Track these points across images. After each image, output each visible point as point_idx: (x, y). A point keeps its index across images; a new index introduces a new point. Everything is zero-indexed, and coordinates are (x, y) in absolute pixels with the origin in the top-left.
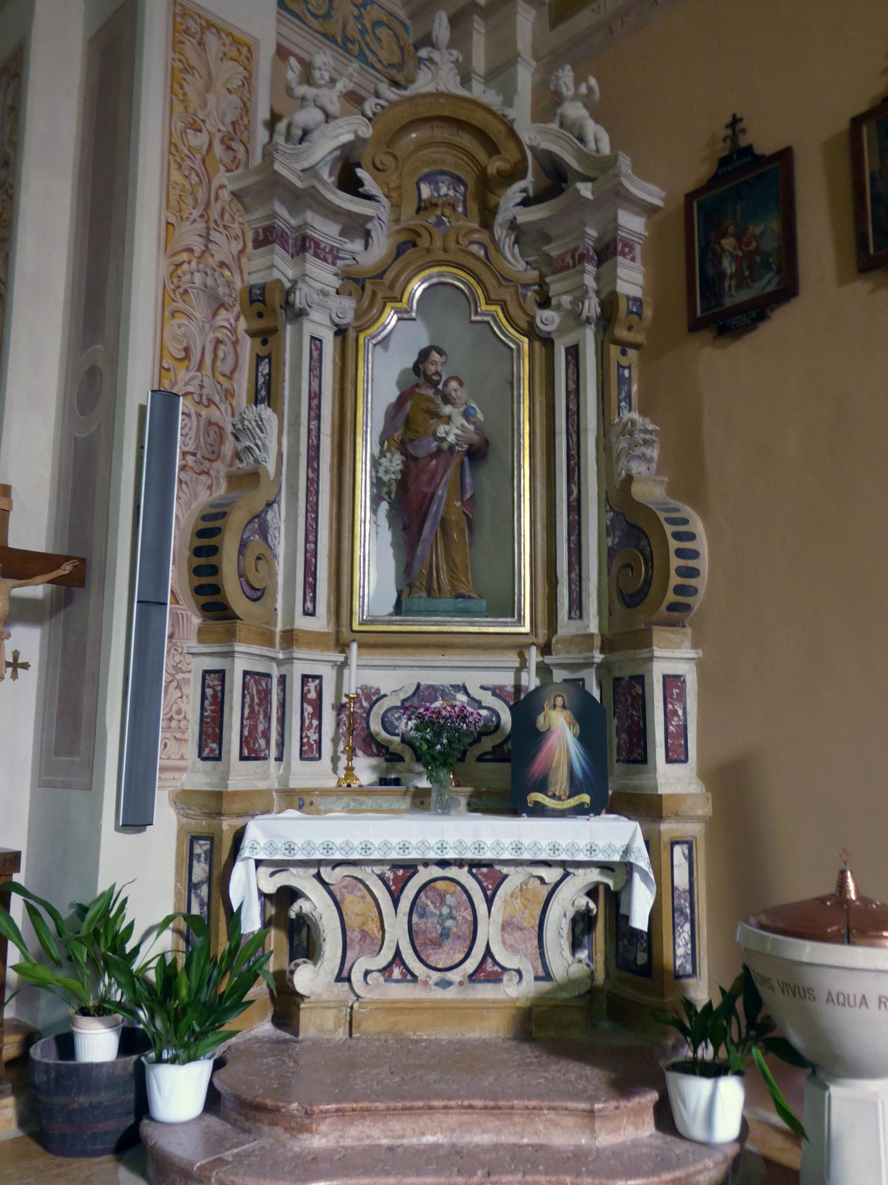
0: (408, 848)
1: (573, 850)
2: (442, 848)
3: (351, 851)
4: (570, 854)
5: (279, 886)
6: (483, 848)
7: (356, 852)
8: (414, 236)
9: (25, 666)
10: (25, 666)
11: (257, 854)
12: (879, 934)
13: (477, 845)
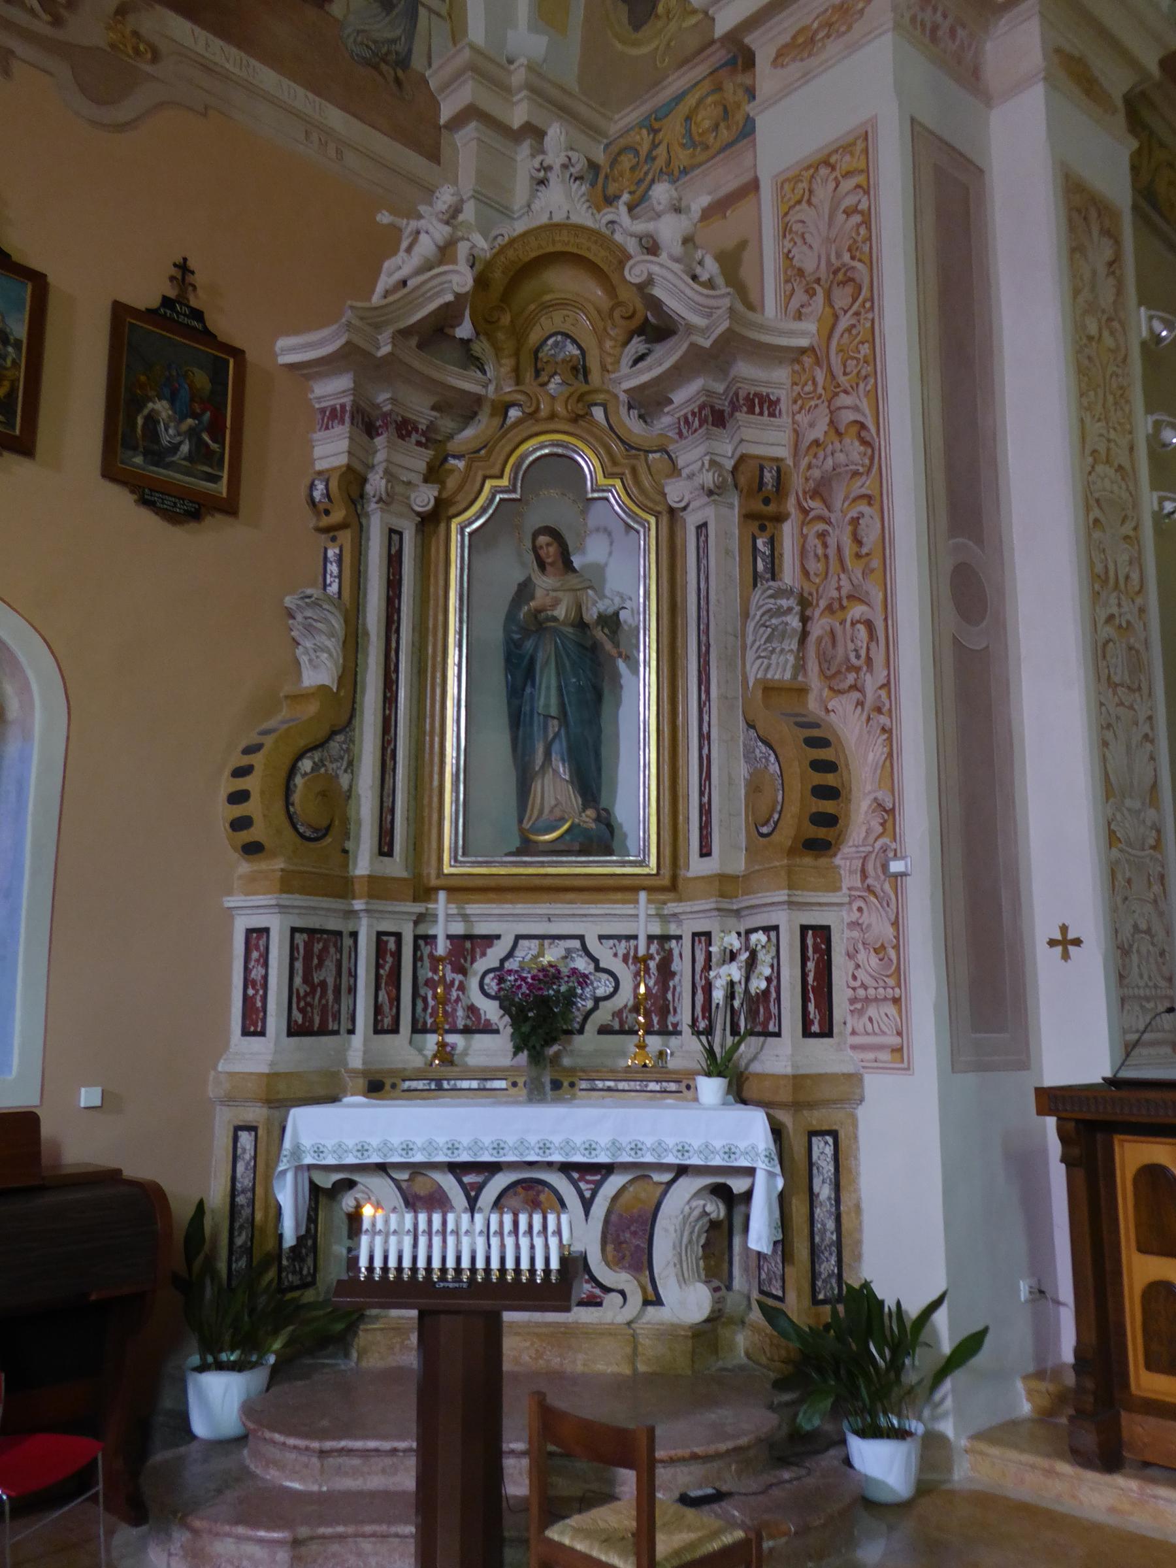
0: (411, 1149)
1: (385, 1150)
2: (683, 1151)
3: (573, 1152)
4: (703, 1157)
5: (158, 1180)
6: (679, 1151)
7: (486, 1152)
8: (1096, 338)
9: (1052, 943)
10: (1052, 943)
11: (736, 1159)
12: (179, 1234)
13: (541, 1145)
